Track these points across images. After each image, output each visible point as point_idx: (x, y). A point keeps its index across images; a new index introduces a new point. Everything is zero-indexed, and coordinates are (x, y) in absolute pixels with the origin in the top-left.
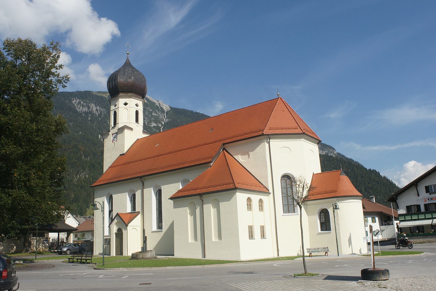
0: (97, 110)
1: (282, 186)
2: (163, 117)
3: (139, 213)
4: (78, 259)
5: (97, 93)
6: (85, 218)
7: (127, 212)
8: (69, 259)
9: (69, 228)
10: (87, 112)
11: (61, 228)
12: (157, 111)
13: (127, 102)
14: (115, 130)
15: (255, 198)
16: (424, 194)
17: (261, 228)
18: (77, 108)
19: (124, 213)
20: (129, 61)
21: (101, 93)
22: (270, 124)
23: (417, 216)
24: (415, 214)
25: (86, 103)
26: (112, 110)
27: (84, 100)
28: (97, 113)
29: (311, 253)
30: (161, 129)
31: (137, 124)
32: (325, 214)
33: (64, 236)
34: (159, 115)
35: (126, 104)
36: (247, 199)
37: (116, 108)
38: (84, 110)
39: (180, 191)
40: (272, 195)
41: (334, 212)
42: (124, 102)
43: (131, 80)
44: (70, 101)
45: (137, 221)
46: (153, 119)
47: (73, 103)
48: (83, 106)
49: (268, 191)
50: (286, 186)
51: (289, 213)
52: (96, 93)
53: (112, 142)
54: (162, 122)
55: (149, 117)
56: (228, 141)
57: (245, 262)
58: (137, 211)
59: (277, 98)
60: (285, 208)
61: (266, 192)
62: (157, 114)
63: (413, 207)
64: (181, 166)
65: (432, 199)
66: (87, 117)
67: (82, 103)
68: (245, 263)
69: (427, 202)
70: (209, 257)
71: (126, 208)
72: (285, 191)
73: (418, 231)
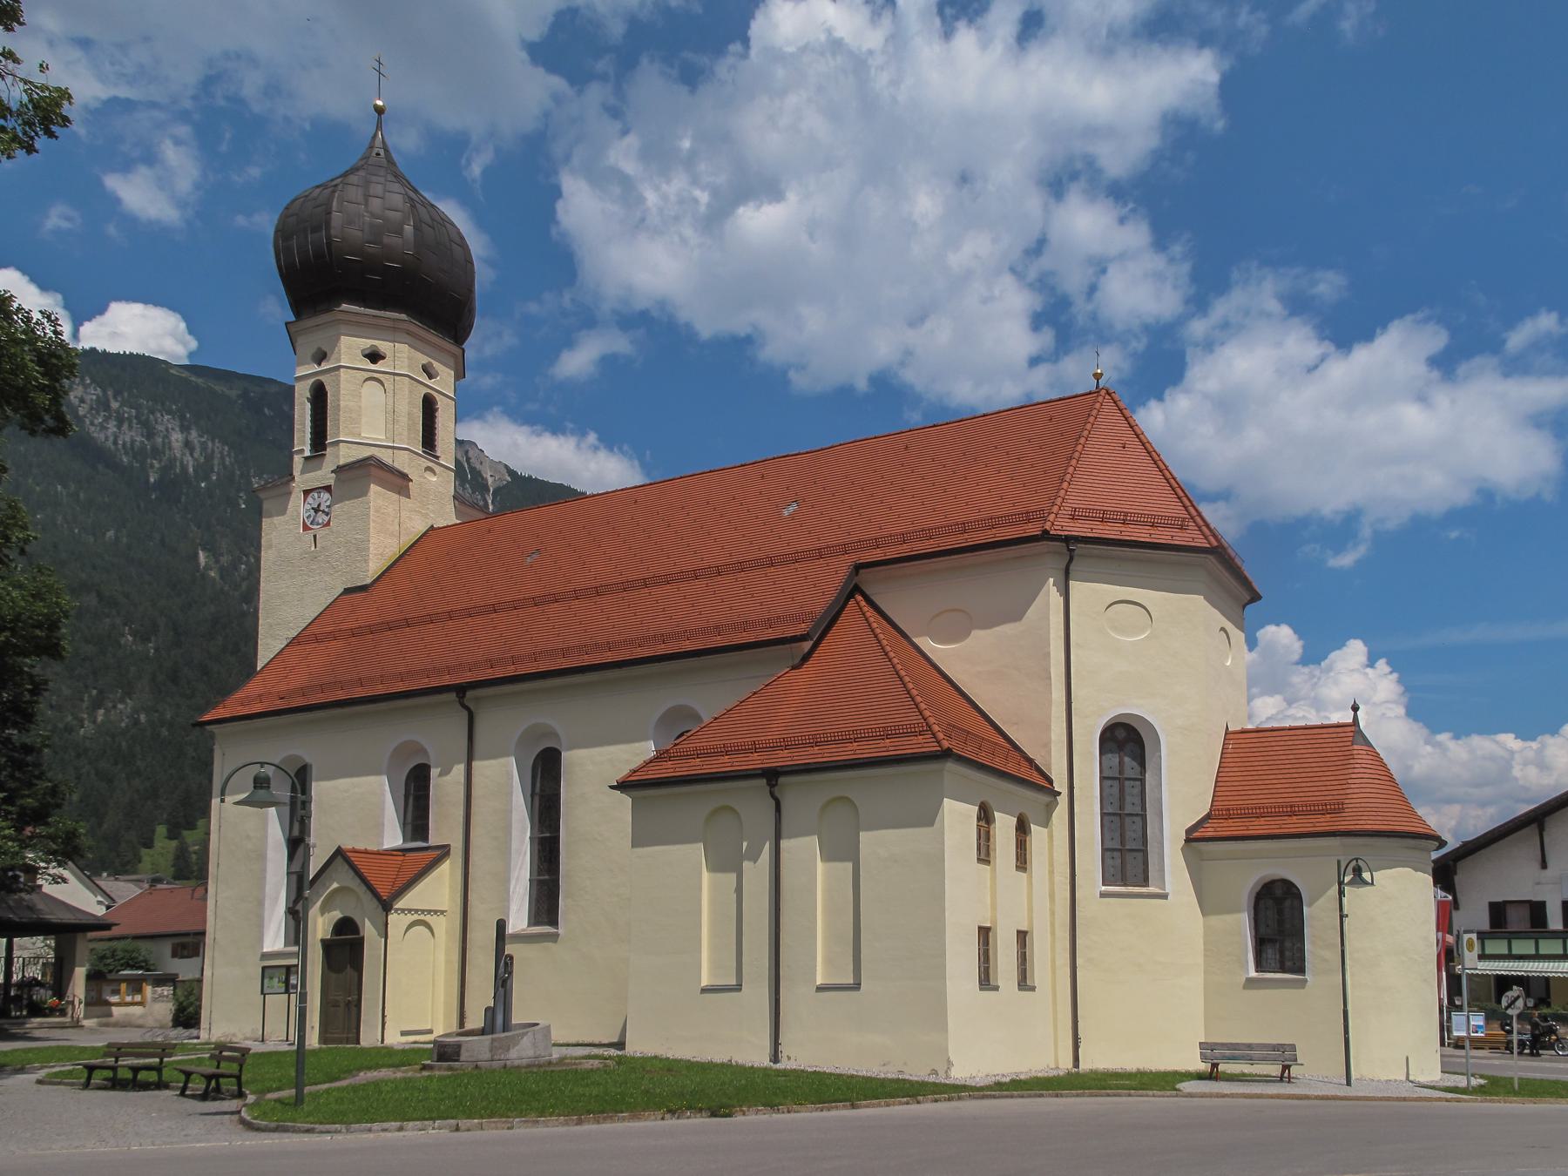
0: (188, 444)
3: (444, 851)
4: (136, 1070)
5: (185, 374)
7: (385, 847)
9: (67, 918)
14: (324, 474)
18: (92, 424)
19: (372, 847)
22: (1075, 498)
23: (1505, 943)
25: (138, 407)
28: (188, 459)
32: (1279, 902)
38: (128, 439)
40: (1063, 800)
45: (438, 888)
48: (120, 421)
50: (1121, 772)
56: (877, 555)
57: (981, 1089)
59: (1094, 389)
60: (1109, 862)
64: (661, 649)
67: (115, 405)
70: (1095, 1059)
71: (379, 827)
72: (1116, 790)
73: (1532, 1000)
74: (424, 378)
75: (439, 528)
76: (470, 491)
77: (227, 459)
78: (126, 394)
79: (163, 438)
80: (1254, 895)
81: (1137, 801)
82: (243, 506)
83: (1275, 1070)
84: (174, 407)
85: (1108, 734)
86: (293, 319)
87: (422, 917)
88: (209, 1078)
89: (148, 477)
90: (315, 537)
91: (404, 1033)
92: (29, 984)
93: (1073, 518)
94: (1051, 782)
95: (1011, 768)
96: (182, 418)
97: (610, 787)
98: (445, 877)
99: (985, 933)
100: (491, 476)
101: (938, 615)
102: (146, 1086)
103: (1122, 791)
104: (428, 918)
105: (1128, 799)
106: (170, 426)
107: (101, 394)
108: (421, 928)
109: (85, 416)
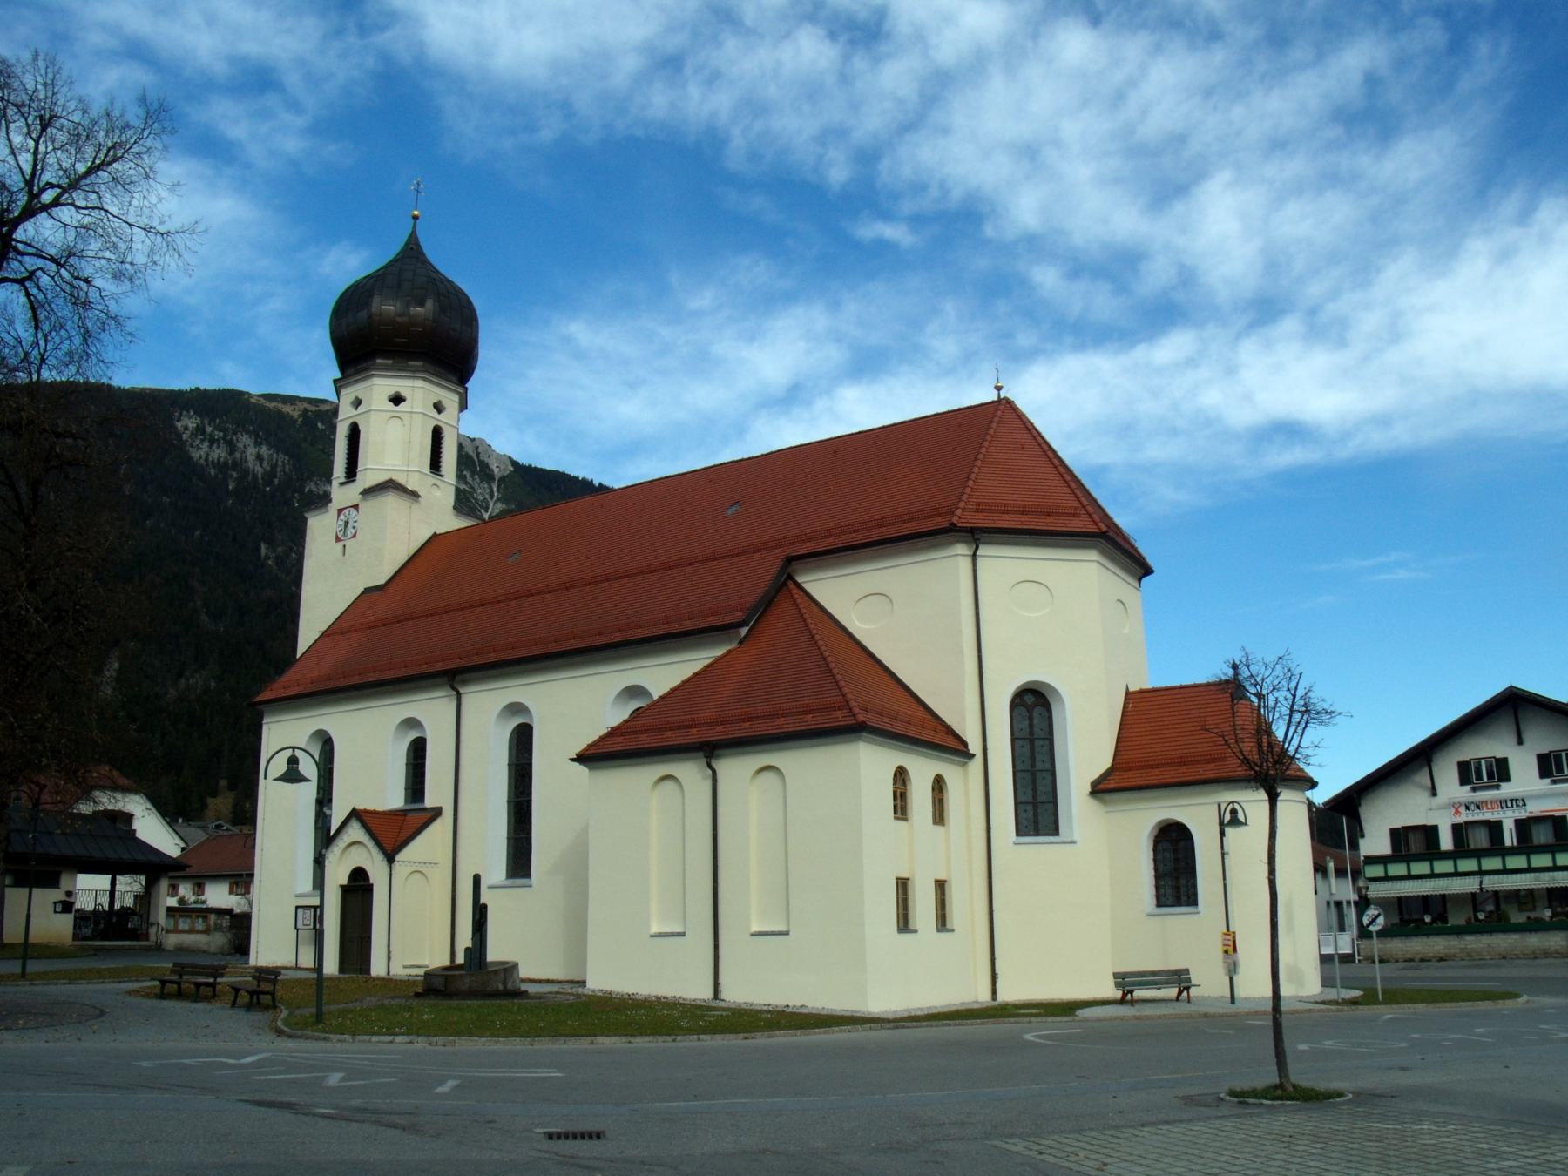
0: (259, 458)
2: (487, 496)
3: (437, 813)
4: (198, 985)
5: (262, 401)
6: (204, 828)
8: (163, 983)
10: (226, 463)
13: (404, 393)
15: (922, 769)
16: (1450, 786)
17: (897, 883)
18: (192, 446)
20: (418, 244)
21: (278, 402)
24: (1419, 858)
25: (224, 430)
26: (342, 420)
27: (218, 421)
29: (1131, 992)
31: (434, 479)
33: (129, 889)
34: (474, 490)
35: (397, 400)
36: (895, 775)
37: (359, 414)
38: (216, 457)
39: (614, 732)
40: (977, 763)
41: (1222, 834)
42: (391, 391)
43: (424, 311)
48: (212, 441)
49: (961, 748)
53: (338, 539)
54: (483, 511)
57: (895, 1020)
58: (430, 802)
61: (950, 745)
62: (466, 483)
63: (1411, 837)
65: (1478, 807)
67: (209, 429)
69: (1465, 817)
70: (737, 993)
74: (434, 413)
75: (440, 534)
76: (478, 480)
77: (287, 466)
78: (218, 421)
79: (241, 454)
80: (1152, 839)
81: (1047, 759)
82: (297, 505)
83: (1173, 992)
84: (251, 428)
85: (1018, 700)
86: (338, 375)
88: (252, 993)
89: (228, 485)
90: (344, 546)
91: (405, 967)
92: (125, 912)
93: (977, 511)
94: (965, 744)
95: (927, 735)
96: (257, 436)
97: (583, 758)
98: (439, 832)
99: (903, 885)
100: (497, 467)
101: (861, 599)
102: (206, 999)
103: (1032, 750)
104: (423, 869)
105: (1038, 758)
106: (247, 444)
107: (200, 423)
108: (418, 876)
109: (187, 441)
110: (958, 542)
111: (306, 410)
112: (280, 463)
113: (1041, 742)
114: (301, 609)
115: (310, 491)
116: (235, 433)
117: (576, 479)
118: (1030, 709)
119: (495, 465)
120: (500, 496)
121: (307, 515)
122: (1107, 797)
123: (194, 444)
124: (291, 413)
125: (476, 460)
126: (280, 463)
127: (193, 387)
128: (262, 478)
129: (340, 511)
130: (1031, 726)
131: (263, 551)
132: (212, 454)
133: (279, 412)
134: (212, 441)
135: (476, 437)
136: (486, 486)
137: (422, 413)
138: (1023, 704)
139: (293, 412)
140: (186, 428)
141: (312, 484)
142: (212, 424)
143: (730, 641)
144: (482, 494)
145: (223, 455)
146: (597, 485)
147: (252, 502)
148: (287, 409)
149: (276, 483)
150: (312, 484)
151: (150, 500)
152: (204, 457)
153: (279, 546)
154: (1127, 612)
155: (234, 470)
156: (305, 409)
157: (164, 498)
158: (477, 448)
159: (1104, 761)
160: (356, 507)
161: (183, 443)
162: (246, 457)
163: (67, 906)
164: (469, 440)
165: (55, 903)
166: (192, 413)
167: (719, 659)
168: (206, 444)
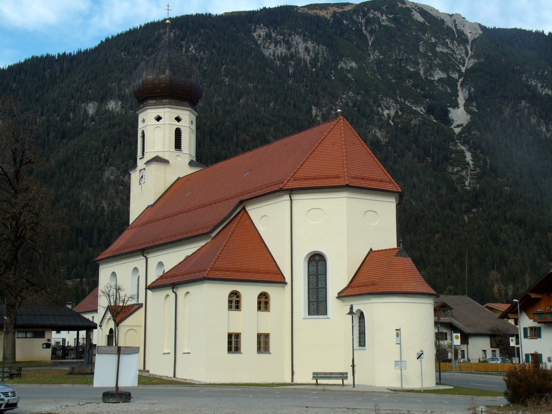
0: (307, 49)
1: (310, 271)
2: (464, 55)
10: (286, 56)
11: (79, 323)
12: (448, 41)
30: (459, 84)
31: (178, 153)
34: (453, 51)
35: (159, 119)
38: (279, 53)
40: (288, 287)
42: (156, 115)
44: (249, 33)
46: (437, 61)
47: (253, 37)
48: (276, 43)
51: (318, 314)
52: (306, 9)
54: (461, 66)
55: (428, 57)
62: (448, 48)
66: (286, 67)
67: (274, 35)
68: (192, 386)
70: (181, 375)
72: (315, 280)
76: (457, 45)
78: (278, 28)
79: (295, 49)
82: (333, 78)
87: (133, 328)
89: (289, 70)
96: (304, 35)
100: (470, 33)
103: (317, 280)
104: (135, 328)
105: (320, 282)
109: (261, 44)
110: (286, 194)
111: (335, 13)
112: (321, 52)
113: (321, 276)
114: (130, 214)
115: (342, 68)
116: (290, 35)
117: (530, 32)
118: (317, 262)
119: (469, 32)
120: (473, 54)
121: (131, 172)
122: (343, 299)
123: (265, 46)
124: (325, 16)
125: (455, 30)
126: (321, 52)
127: (262, 8)
128: (310, 63)
129: (140, 171)
130: (317, 269)
131: (314, 112)
132: (276, 51)
133: (318, 16)
134: (276, 43)
135: (454, 13)
136: (462, 48)
137: (169, 124)
138: (314, 260)
139: (326, 14)
140: (260, 36)
141: (342, 63)
142: (276, 32)
143: (207, 239)
144: (460, 54)
145: (284, 51)
146: (547, 34)
147: (305, 79)
148: (322, 13)
149: (319, 65)
150: (342, 63)
151: (241, 86)
152: (272, 53)
153: (323, 107)
154: (378, 215)
155: (292, 60)
156: (334, 11)
157: (249, 84)
158: (455, 21)
159: (345, 283)
160: (144, 169)
161: (258, 46)
162: (298, 50)
163: (48, 346)
164: (449, 17)
165: (43, 344)
166: (262, 26)
167: (203, 246)
168: (273, 45)
